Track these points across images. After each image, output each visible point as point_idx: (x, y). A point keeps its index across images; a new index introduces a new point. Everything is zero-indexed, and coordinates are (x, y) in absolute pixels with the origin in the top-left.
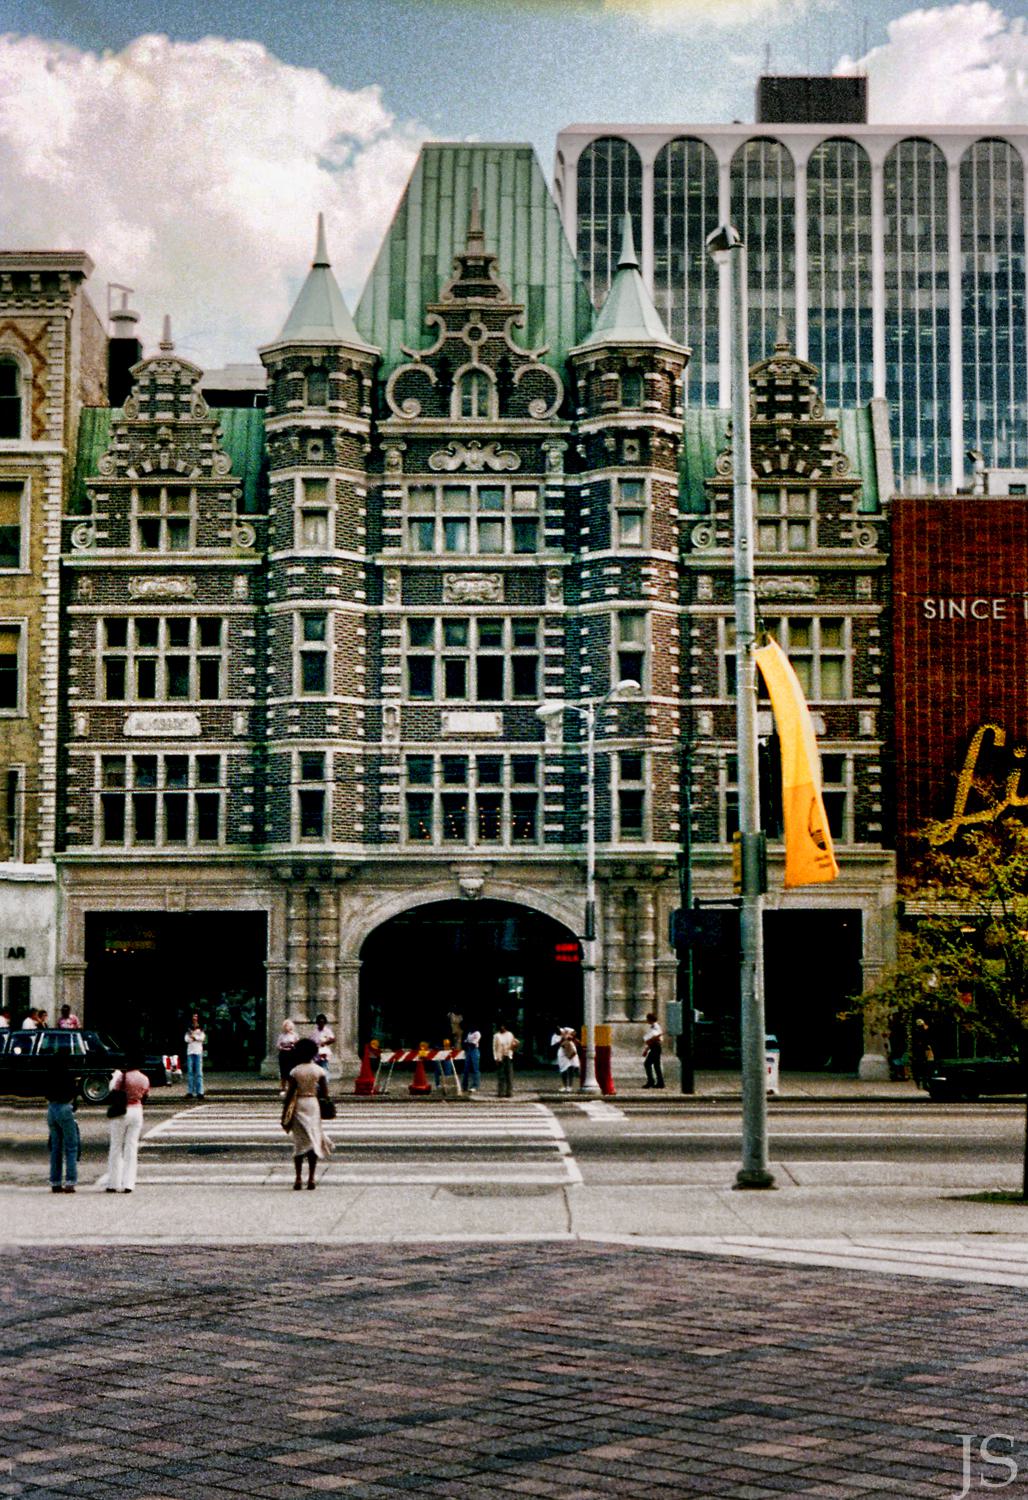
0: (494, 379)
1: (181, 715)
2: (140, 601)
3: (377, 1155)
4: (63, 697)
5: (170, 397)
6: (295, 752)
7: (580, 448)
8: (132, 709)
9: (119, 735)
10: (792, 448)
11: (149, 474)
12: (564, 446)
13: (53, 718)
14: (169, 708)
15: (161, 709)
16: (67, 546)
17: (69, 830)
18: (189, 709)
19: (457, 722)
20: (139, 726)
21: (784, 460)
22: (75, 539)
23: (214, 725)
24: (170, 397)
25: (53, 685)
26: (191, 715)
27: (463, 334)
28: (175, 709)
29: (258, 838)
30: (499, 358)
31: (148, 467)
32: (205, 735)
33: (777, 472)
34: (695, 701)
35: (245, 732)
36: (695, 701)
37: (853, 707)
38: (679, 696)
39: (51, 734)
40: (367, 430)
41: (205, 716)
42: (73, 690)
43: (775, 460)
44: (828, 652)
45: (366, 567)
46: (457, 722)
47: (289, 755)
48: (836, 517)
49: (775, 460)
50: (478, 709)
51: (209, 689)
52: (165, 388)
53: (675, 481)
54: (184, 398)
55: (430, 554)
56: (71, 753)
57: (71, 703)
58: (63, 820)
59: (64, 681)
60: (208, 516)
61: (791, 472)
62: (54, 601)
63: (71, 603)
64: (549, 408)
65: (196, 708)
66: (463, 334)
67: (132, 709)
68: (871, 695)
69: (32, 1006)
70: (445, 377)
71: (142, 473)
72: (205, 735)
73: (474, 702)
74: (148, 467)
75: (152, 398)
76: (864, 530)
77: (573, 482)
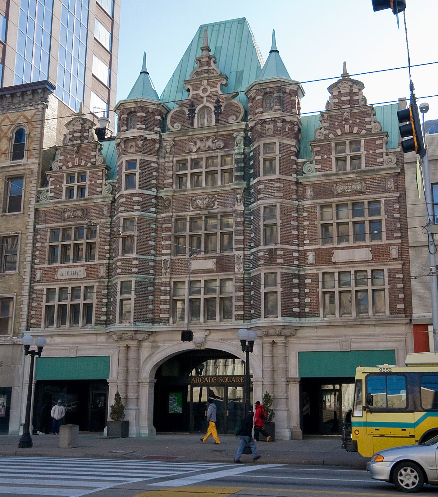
0: (213, 109)
1: (78, 269)
2: (338, 195)
3: (236, 483)
4: (33, 263)
5: (79, 134)
6: (279, 272)
7: (249, 134)
8: (59, 267)
9: (329, 262)
10: (351, 122)
11: (71, 167)
12: (243, 134)
13: (28, 273)
14: (74, 266)
15: (71, 267)
16: (38, 200)
17: (32, 321)
18: (82, 266)
19: (196, 265)
20: (62, 275)
21: (347, 127)
22: (42, 197)
23: (91, 272)
24: (348, 98)
25: (29, 259)
26: (82, 269)
27: (200, 92)
28: (77, 266)
29: (107, 323)
30: (216, 99)
31: (70, 165)
32: (88, 277)
33: (343, 133)
34: (306, 248)
35: (104, 275)
36: (306, 248)
37: (387, 245)
38: (298, 245)
39: (27, 280)
40: (158, 138)
41: (88, 269)
42: (37, 261)
43: (342, 129)
44: (356, 219)
45: (156, 197)
46: (196, 265)
47: (43, 290)
48: (374, 152)
49: (342, 129)
50: (205, 258)
51: (90, 256)
52: (345, 95)
53: (294, 144)
54: (355, 98)
55: (345, 171)
56: (35, 288)
57: (36, 266)
58: (29, 316)
59: (34, 257)
60: (93, 182)
61: (351, 132)
62: (32, 223)
63: (38, 224)
64: (237, 119)
65: (85, 265)
66: (200, 92)
67: (59, 267)
68: (396, 238)
69: (206, 400)
70: (192, 111)
71: (68, 167)
72: (88, 277)
73: (351, 244)
74: (70, 165)
75: (83, 135)
76: (390, 156)
77: (247, 151)
